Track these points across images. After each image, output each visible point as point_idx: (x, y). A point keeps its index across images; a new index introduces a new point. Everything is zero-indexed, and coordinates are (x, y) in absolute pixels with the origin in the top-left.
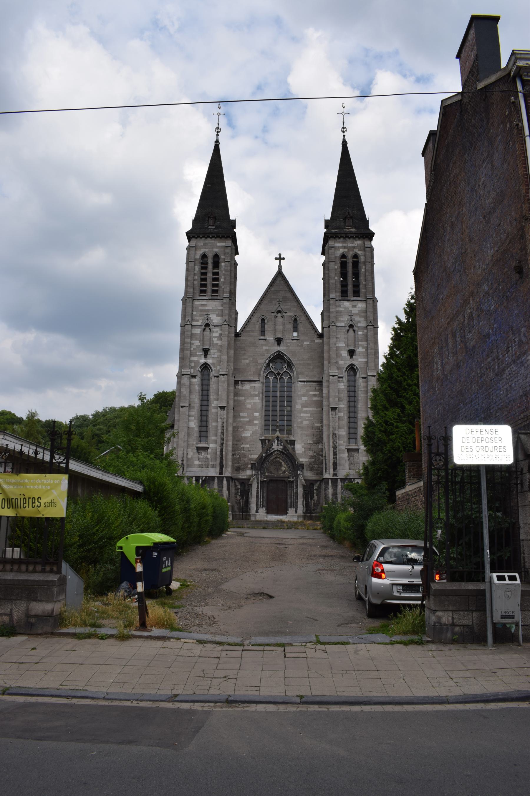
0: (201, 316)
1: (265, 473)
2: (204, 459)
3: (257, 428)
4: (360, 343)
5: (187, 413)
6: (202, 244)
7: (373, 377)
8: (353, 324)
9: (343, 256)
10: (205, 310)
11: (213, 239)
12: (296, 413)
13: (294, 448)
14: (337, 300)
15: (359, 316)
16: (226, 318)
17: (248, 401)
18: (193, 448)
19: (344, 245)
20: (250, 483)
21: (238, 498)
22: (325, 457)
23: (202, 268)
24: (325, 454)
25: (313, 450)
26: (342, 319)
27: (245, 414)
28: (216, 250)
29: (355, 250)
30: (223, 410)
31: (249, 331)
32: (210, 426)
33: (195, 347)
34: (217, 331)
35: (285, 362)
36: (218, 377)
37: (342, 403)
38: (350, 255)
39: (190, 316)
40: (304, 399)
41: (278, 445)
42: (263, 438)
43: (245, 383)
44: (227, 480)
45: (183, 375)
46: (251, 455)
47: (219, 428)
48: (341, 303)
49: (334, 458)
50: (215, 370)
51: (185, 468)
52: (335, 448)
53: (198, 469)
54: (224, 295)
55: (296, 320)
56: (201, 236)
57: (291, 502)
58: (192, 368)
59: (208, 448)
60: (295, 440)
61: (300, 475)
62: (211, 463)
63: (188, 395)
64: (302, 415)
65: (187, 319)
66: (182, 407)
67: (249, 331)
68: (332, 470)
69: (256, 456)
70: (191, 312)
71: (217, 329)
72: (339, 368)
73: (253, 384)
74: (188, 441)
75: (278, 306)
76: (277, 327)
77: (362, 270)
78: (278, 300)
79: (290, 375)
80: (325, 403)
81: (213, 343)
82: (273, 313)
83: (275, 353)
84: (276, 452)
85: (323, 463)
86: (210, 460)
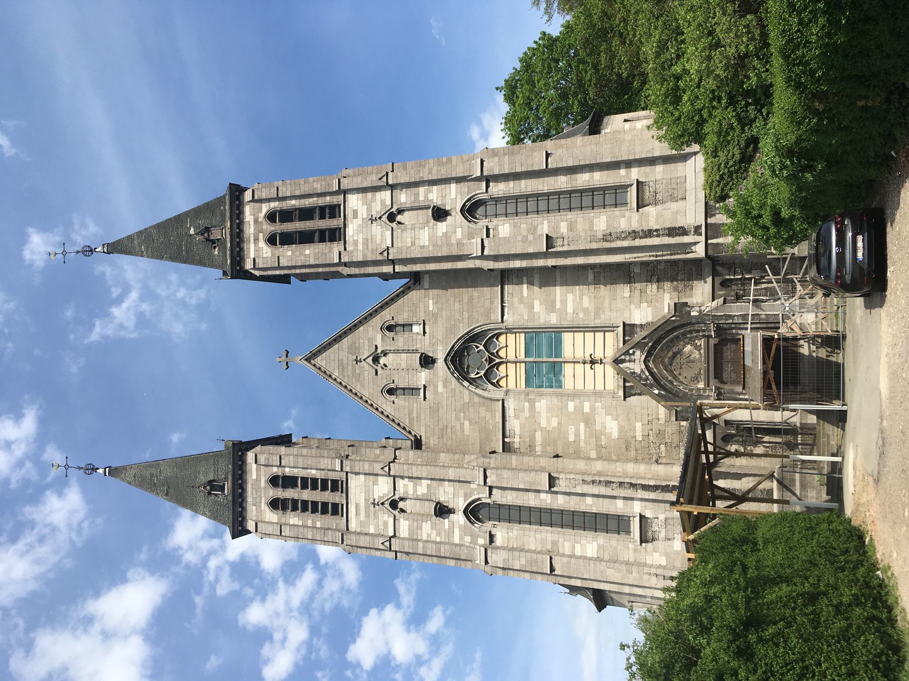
0: (376, 517)
1: (699, 389)
2: (669, 527)
3: (598, 404)
4: (421, 198)
5: (565, 559)
6: (254, 508)
7: (485, 164)
9: (271, 240)
10: (367, 508)
13: (641, 325)
14: (345, 249)
18: (643, 551)
19: (252, 241)
21: (759, 450)
23: (295, 509)
26: (379, 237)
27: (572, 430)
28: (263, 483)
29: (261, 219)
30: (557, 481)
33: (434, 532)
34: (404, 485)
36: (491, 488)
37: (540, 227)
38: (269, 228)
39: (376, 540)
40: (537, 307)
43: (507, 429)
45: (486, 562)
46: (658, 419)
48: (351, 240)
49: (658, 236)
50: (478, 494)
54: (337, 469)
55: (390, 328)
58: (474, 542)
59: (642, 517)
60: (624, 323)
61: (700, 311)
63: (528, 555)
64: (570, 310)
65: (381, 547)
67: (411, 420)
69: (662, 411)
70: (367, 538)
71: (400, 483)
72: (471, 236)
73: (510, 413)
74: (627, 563)
76: (404, 365)
78: (355, 362)
79: (492, 337)
82: (376, 372)
83: (449, 369)
84: (651, 365)
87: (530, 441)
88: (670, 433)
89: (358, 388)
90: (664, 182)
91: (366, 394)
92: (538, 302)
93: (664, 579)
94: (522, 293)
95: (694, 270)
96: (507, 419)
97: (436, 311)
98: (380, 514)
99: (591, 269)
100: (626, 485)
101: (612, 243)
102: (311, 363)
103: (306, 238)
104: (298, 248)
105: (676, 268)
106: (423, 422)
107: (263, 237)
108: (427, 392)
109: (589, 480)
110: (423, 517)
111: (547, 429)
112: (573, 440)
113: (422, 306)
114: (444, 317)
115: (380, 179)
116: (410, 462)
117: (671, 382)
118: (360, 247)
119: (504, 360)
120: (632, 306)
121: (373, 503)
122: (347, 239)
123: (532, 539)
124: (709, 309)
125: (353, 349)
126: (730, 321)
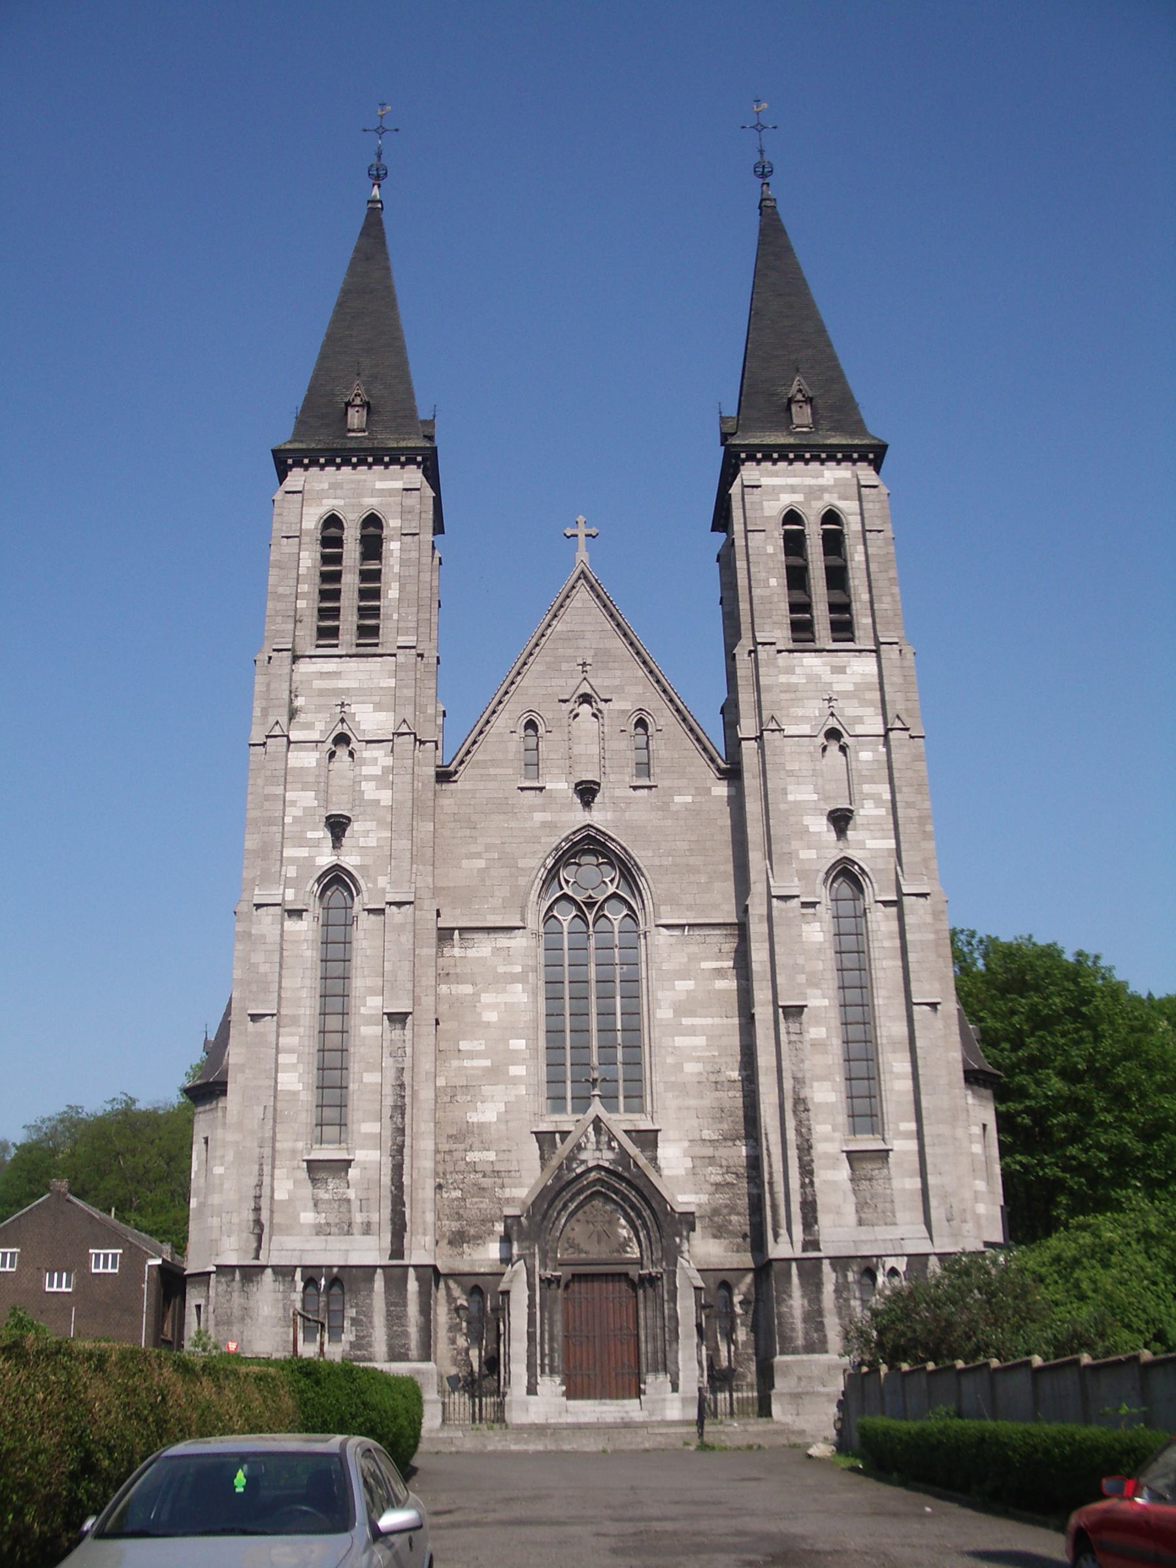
0: (319, 709)
4: (867, 788)
5: (272, 1038)
6: (326, 486)
7: (922, 900)
9: (792, 517)
12: (656, 1034)
14: (779, 652)
15: (856, 701)
16: (408, 712)
17: (486, 998)
21: (462, 1342)
23: (326, 559)
24: (771, 1174)
25: (724, 1163)
26: (800, 712)
27: (479, 1045)
29: (827, 496)
30: (398, 1026)
33: (299, 813)
34: (377, 758)
35: (611, 864)
36: (381, 911)
37: (818, 992)
42: (544, 1127)
44: (418, 1279)
45: (258, 906)
46: (503, 1187)
47: (388, 1090)
48: (796, 662)
49: (803, 1185)
50: (368, 889)
51: (265, 1237)
53: (318, 1242)
55: (641, 723)
56: (322, 460)
57: (655, 1353)
59: (348, 1163)
60: (657, 1131)
62: (358, 1218)
64: (680, 1041)
66: (255, 1017)
67: (483, 764)
68: (801, 1228)
72: (803, 875)
73: (502, 940)
79: (630, 908)
82: (565, 701)
83: (574, 833)
84: (593, 1175)
86: (355, 1205)
87: (456, 974)
88: (481, 1206)
89: (536, 667)
90: (888, 1191)
91: (524, 682)
92: (692, 987)
93: (255, 1197)
94: (706, 959)
96: (492, 936)
97: (674, 808)
100: (399, 1139)
101: (791, 1113)
102: (577, 581)
103: (797, 578)
109: (404, 1079)
110: (325, 796)
111: (477, 1004)
112: (461, 1048)
113: (682, 783)
115: (898, 717)
116: (416, 768)
118: (783, 679)
119: (591, 929)
120: (686, 1144)
121: (343, 703)
123: (298, 982)
124: (685, 1264)
125: (604, 658)
126: (666, 1297)
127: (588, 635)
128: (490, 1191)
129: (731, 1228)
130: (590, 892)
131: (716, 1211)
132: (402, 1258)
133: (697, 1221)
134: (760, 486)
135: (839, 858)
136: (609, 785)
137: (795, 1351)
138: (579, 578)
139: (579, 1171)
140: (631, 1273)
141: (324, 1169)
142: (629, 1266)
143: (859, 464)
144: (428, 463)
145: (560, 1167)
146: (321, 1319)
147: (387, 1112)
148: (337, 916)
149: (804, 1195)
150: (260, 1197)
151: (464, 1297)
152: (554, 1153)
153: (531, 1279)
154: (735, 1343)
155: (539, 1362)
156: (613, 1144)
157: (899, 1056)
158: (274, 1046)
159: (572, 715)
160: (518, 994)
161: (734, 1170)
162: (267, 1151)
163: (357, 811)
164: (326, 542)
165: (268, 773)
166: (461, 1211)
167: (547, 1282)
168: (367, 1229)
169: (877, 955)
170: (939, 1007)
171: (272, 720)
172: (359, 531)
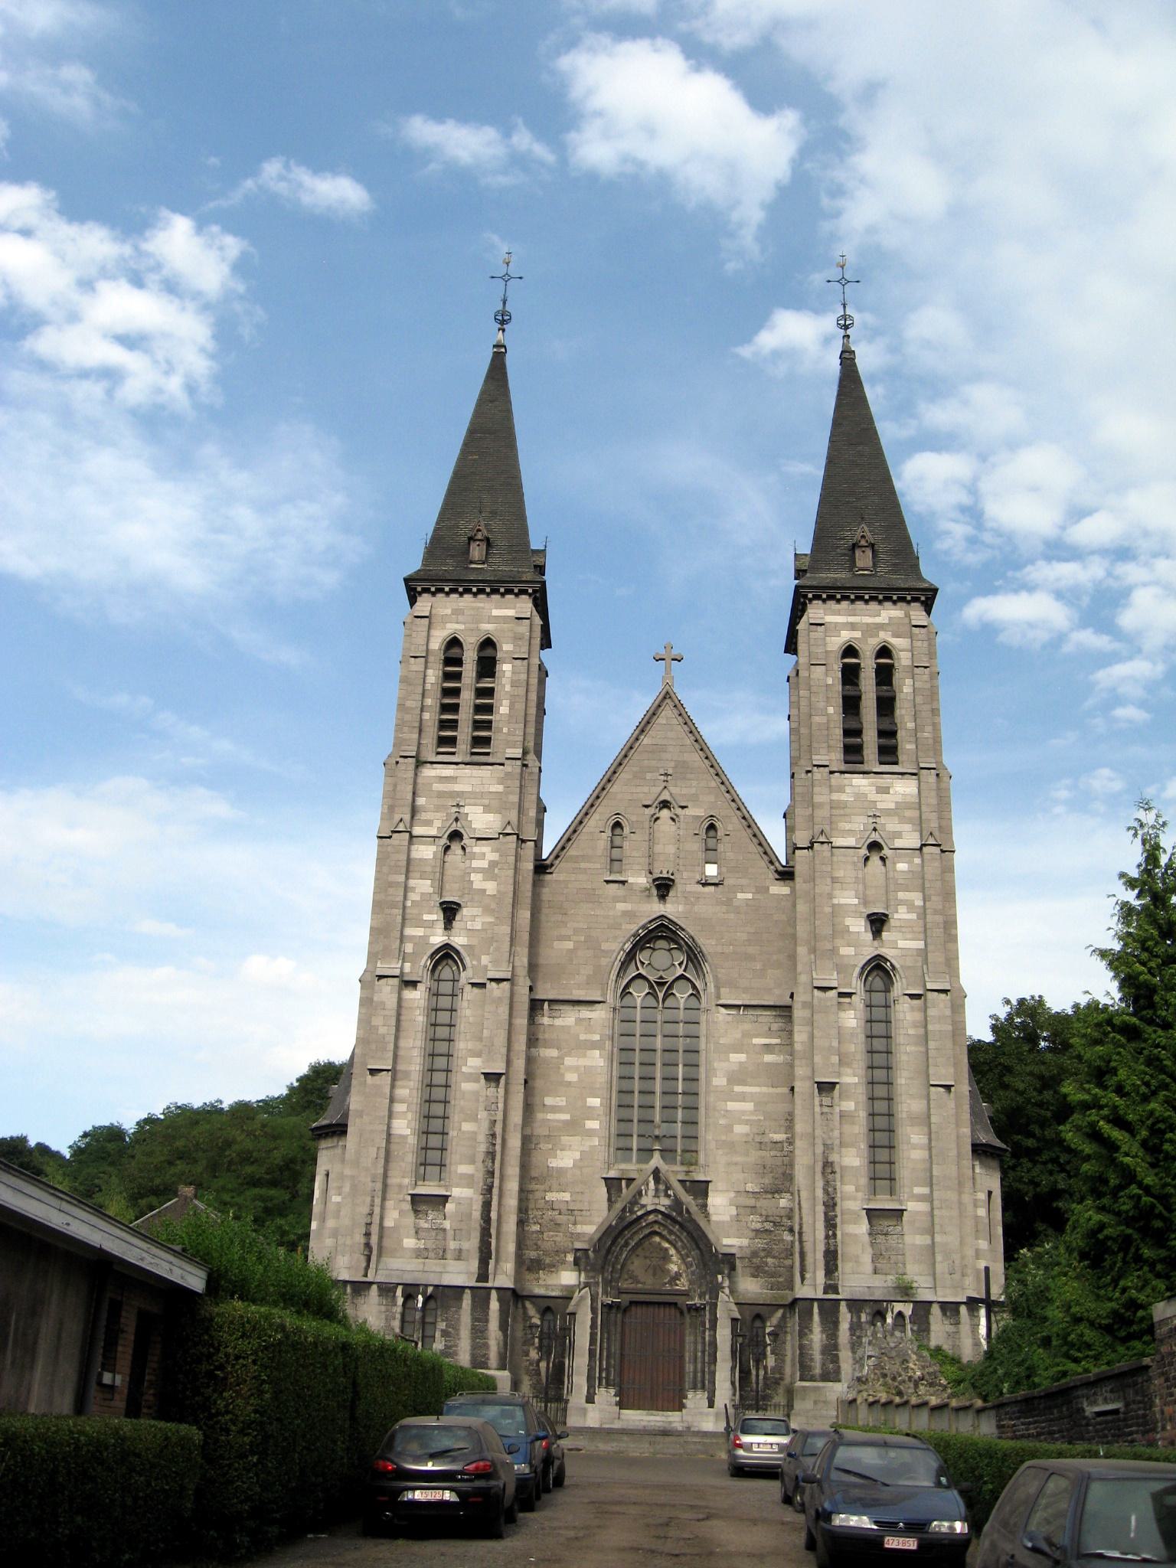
0: (438, 809)
4: (901, 895)
6: (449, 611)
7: (943, 996)
8: (880, 841)
9: (850, 651)
10: (453, 794)
11: (482, 596)
14: (832, 772)
17: (569, 1061)
18: (401, 1197)
19: (851, 619)
20: (570, 1309)
22: (800, 1234)
24: (801, 1225)
25: (764, 1213)
26: (848, 826)
27: (561, 1101)
30: (493, 1084)
31: (577, 856)
32: (453, 1133)
33: (418, 899)
34: (484, 854)
35: (680, 948)
36: (482, 985)
37: (849, 1071)
41: (656, 1196)
42: (612, 1174)
44: (499, 1300)
45: (380, 977)
46: (575, 1224)
47: (482, 1138)
48: (846, 782)
49: (827, 1237)
51: (374, 1258)
52: (830, 1205)
55: (712, 827)
57: (695, 1372)
59: (445, 1198)
62: (452, 1245)
64: (732, 1106)
66: (373, 1072)
67: (576, 859)
68: (823, 1272)
72: (841, 968)
73: (585, 1013)
75: (661, 788)
77: (905, 687)
79: (694, 987)
80: (800, 1071)
81: (471, 888)
82: (647, 806)
84: (651, 1218)
85: (792, 1255)
86: (450, 1234)
90: (901, 1246)
94: (757, 1036)
95: (781, 1280)
96: (577, 1008)
97: (736, 903)
98: (441, 815)
99: (788, 1138)
100: (489, 1180)
103: (851, 705)
104: (837, 695)
105: (783, 1255)
106: (573, 877)
107: (855, 639)
108: (616, 885)
111: (562, 1066)
112: (546, 1103)
113: (744, 882)
114: (726, 916)
115: (931, 834)
117: (627, 1244)
119: (661, 1005)
120: (732, 1195)
122: (846, 775)
125: (683, 768)
126: (707, 1326)
127: (671, 749)
128: (563, 1227)
129: (766, 1268)
130: (661, 973)
131: (755, 1254)
132: (487, 1282)
133: (737, 1261)
134: (823, 624)
135: (873, 955)
136: (682, 881)
137: (812, 1379)
138: (665, 698)
139: (639, 1213)
140: (679, 1302)
141: (426, 1203)
142: (678, 1297)
143: (912, 604)
144: (538, 595)
145: (624, 1210)
146: (416, 1339)
147: (480, 1157)
148: (446, 987)
149: (828, 1244)
150: (370, 1224)
151: (538, 1316)
152: (620, 1197)
153: (595, 1304)
154: (765, 1368)
155: (597, 1375)
156: (669, 1192)
157: (916, 1129)
158: (388, 1096)
159: (653, 819)
160: (597, 1060)
161: (771, 1219)
162: (379, 1186)
163: (466, 898)
164: (448, 661)
165: (393, 863)
166: (539, 1243)
167: (610, 1307)
168: (459, 1255)
169: (902, 1041)
170: (953, 1089)
171: (397, 817)
172: (476, 653)
